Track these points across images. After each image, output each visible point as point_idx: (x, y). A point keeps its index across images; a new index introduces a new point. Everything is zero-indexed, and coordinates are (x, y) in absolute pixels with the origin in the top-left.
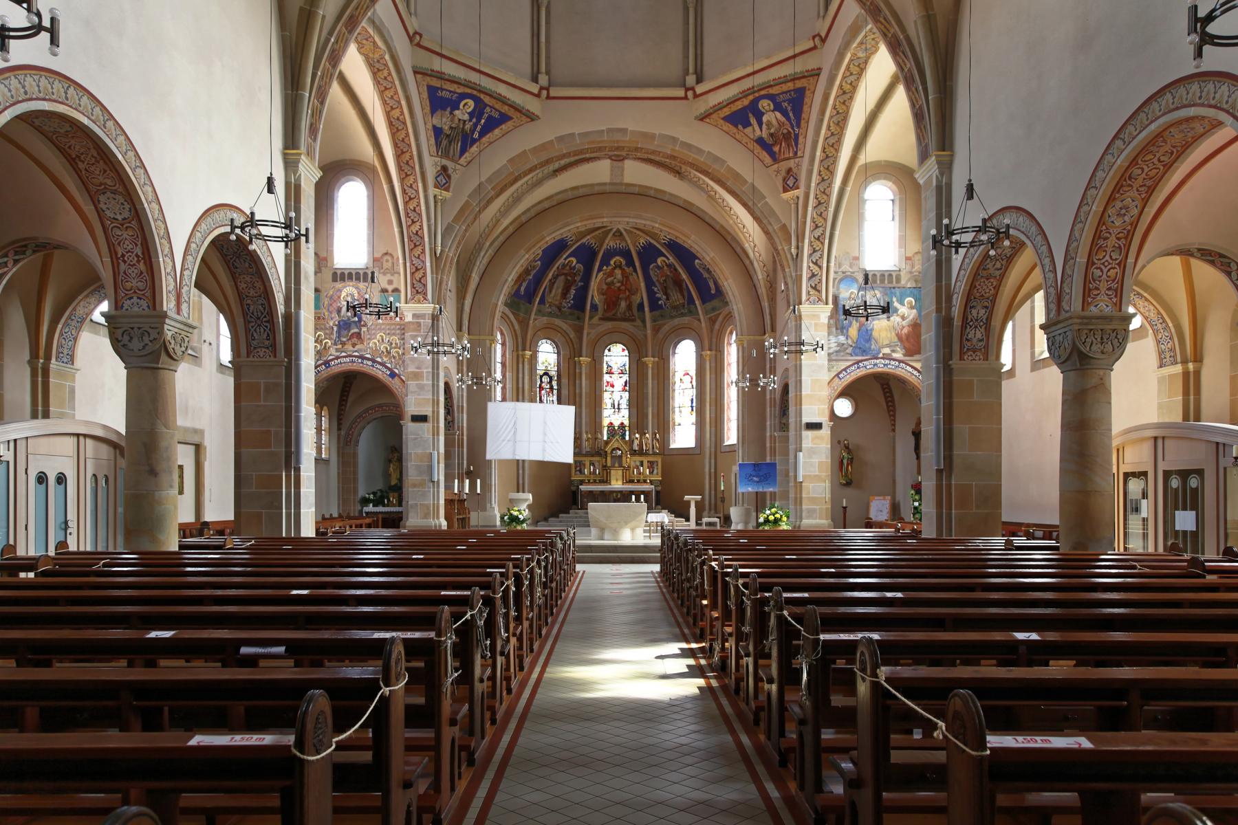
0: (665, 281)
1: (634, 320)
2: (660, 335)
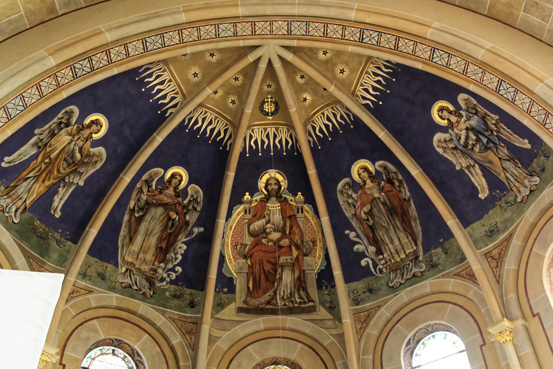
0: (370, 213)
1: (312, 310)
2: (373, 330)
